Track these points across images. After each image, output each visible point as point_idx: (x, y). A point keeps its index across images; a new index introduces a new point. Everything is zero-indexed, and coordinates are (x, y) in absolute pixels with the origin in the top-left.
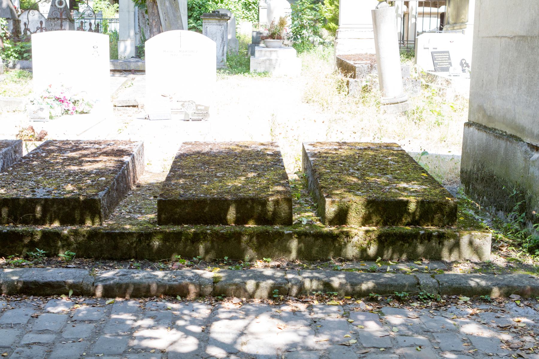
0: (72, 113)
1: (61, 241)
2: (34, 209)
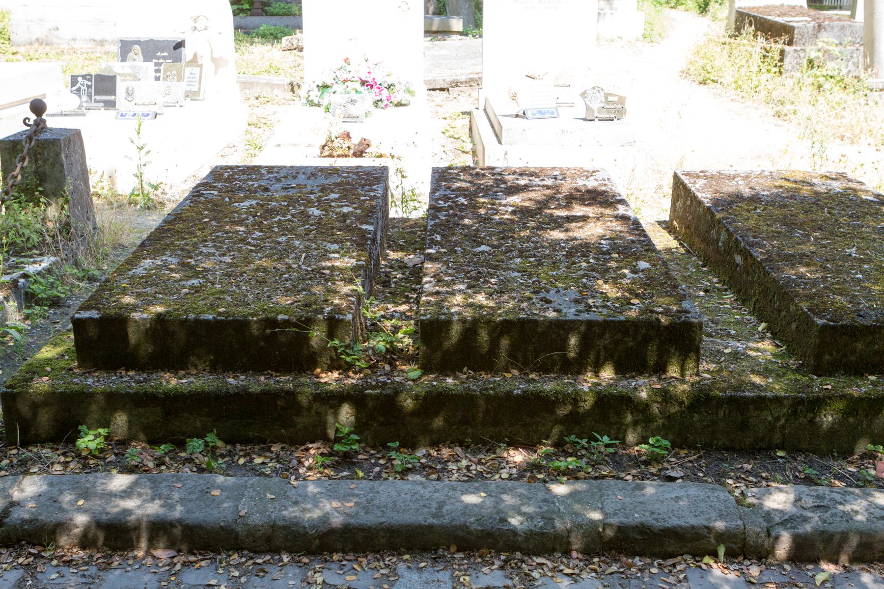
0: (386, 106)
1: (632, 413)
2: (565, 340)
